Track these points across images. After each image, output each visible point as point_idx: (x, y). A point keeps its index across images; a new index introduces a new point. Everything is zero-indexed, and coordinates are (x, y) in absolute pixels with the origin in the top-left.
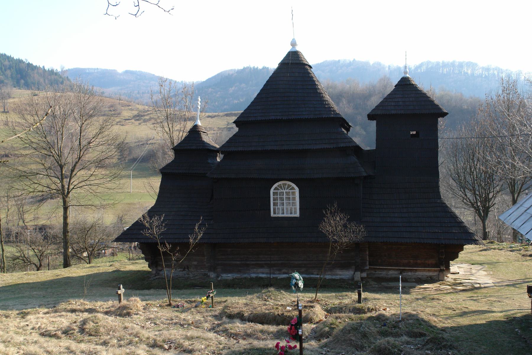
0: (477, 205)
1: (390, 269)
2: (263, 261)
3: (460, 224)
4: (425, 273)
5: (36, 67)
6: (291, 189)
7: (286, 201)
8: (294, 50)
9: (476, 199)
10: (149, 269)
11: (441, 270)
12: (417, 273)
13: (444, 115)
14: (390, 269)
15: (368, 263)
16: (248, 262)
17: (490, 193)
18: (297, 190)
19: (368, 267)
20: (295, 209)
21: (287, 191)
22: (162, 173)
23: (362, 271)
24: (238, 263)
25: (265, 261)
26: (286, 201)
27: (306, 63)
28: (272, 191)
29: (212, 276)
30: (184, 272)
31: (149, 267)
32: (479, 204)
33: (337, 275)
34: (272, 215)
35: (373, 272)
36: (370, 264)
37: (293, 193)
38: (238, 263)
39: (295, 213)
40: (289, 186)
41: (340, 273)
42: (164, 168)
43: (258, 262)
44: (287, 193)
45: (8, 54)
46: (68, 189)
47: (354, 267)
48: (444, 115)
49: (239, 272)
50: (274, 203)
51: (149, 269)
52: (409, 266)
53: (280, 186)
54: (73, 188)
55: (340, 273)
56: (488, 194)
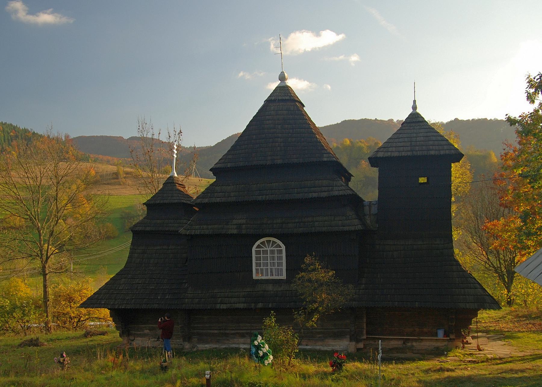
0: (501, 270)
1: (392, 339)
2: (244, 330)
3: (466, 278)
4: (432, 343)
5: (41, 136)
6: (276, 247)
7: (269, 261)
8: (283, 85)
9: (500, 263)
10: (120, 339)
11: (450, 339)
12: (423, 344)
13: (458, 156)
14: (392, 339)
15: (365, 332)
16: (227, 332)
17: (516, 256)
18: (283, 247)
19: (365, 337)
20: (282, 270)
21: (272, 249)
22: (132, 231)
23: (358, 341)
24: (216, 332)
25: (246, 330)
26: (269, 261)
27: (297, 99)
28: (254, 249)
29: (187, 347)
30: (158, 342)
31: (121, 336)
32: (503, 269)
33: (329, 345)
34: (255, 277)
35: (372, 342)
36: (368, 333)
37: (280, 252)
38: (216, 332)
39: (282, 275)
40: (274, 243)
41: (333, 343)
42: (135, 226)
43: (238, 331)
44: (272, 252)
45: (14, 124)
46: (47, 255)
47: (348, 336)
48: (458, 156)
49: (218, 342)
50: (256, 263)
51: (246, 357)
52: (414, 336)
53: (263, 243)
54: (52, 254)
55: (333, 343)
56: (514, 258)
